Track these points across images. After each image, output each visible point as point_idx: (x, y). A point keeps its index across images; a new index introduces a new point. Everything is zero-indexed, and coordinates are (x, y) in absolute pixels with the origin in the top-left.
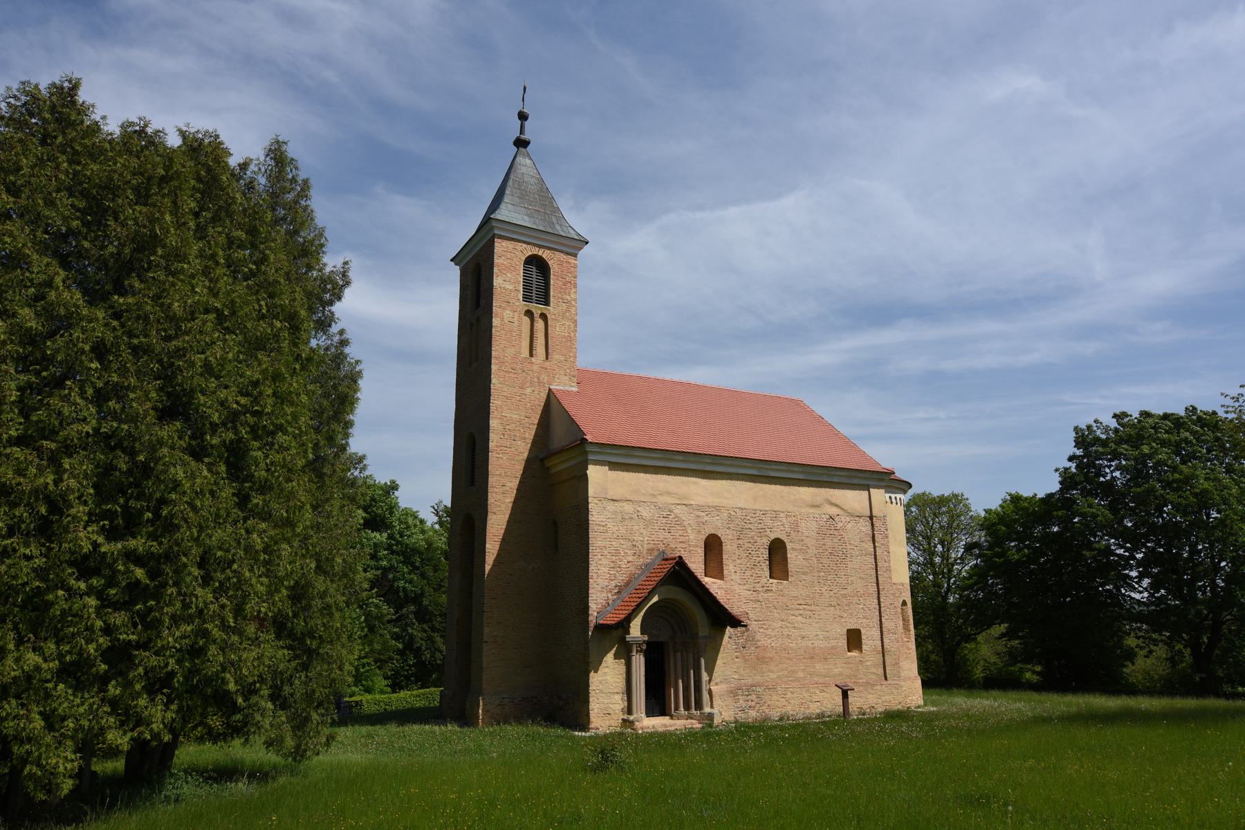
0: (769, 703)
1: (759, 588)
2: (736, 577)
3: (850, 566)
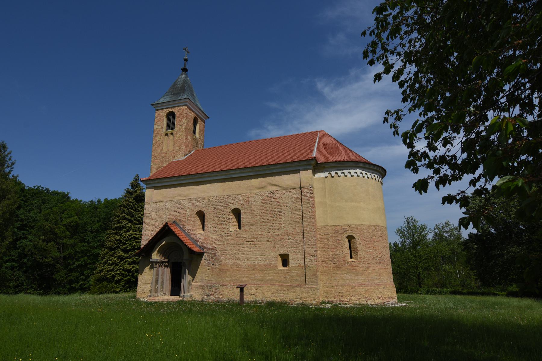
0: (222, 293)
1: (223, 234)
2: (211, 230)
3: (283, 218)
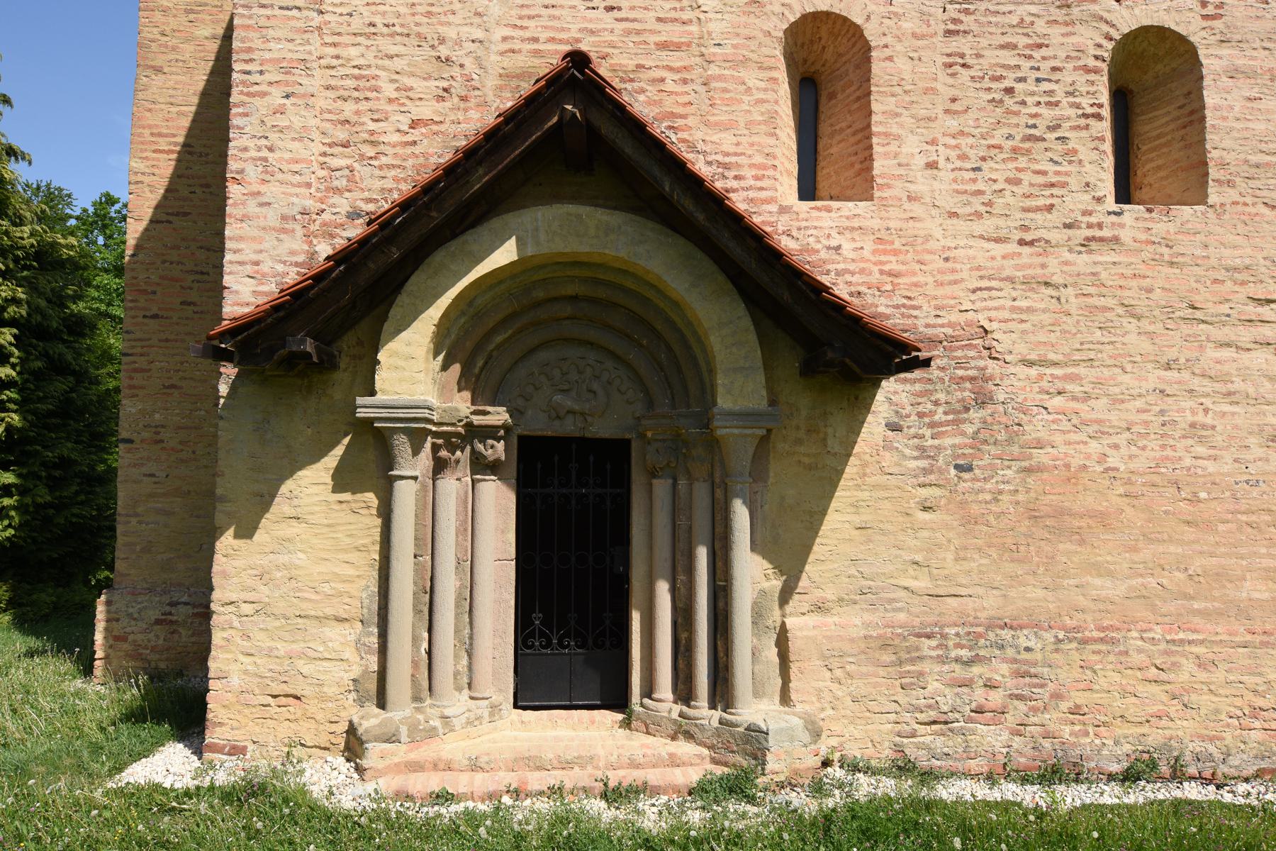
0: (1080, 698)
2: (941, 187)
